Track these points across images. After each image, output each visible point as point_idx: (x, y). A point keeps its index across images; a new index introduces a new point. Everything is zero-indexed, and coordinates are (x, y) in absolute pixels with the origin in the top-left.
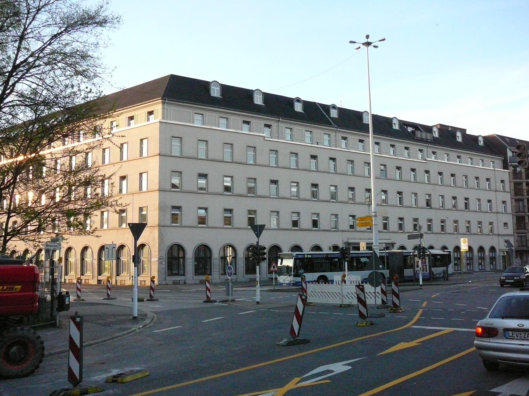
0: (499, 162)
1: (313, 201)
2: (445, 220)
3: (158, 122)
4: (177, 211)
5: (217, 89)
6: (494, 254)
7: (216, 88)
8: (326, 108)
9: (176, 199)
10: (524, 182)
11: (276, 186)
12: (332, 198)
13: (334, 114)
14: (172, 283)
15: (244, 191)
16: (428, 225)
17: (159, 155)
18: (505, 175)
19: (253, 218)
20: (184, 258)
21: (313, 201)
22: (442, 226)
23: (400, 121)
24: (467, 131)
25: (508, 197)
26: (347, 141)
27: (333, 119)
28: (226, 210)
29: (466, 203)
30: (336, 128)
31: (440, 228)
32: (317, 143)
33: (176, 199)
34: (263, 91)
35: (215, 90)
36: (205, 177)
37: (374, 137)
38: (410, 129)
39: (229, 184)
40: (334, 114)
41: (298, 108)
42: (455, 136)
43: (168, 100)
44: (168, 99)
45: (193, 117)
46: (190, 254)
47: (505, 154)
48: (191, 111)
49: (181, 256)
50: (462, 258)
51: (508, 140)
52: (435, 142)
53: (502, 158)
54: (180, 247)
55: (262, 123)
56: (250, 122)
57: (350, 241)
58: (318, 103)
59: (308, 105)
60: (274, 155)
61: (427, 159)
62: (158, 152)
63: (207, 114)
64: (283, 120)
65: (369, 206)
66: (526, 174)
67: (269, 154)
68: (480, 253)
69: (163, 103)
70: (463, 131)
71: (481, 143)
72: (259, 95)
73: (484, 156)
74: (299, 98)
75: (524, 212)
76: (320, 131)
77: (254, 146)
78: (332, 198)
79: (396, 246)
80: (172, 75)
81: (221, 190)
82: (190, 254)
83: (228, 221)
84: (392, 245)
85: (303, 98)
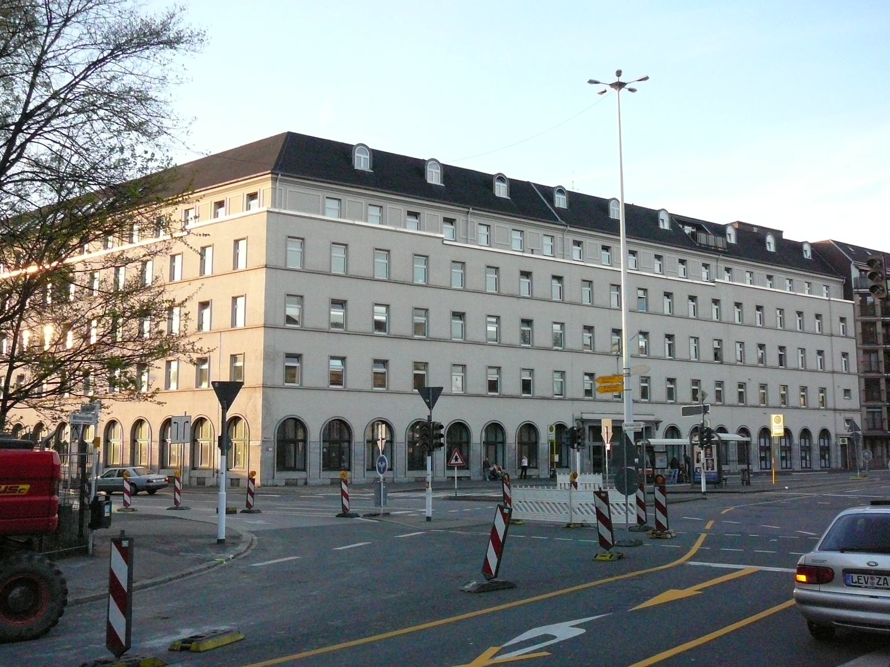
0: (836, 286)
1: (523, 348)
2: (745, 383)
3: (265, 212)
4: (293, 362)
5: (364, 158)
6: (767, 440)
7: (363, 156)
8: (548, 192)
9: (294, 342)
10: (878, 320)
11: (461, 322)
12: (555, 344)
13: (561, 202)
14: (284, 484)
15: (408, 331)
16: (717, 391)
17: (266, 266)
18: (848, 307)
19: (423, 375)
20: (305, 441)
21: (523, 348)
22: (741, 394)
23: (813, 245)
24: (783, 234)
25: (851, 346)
26: (582, 248)
27: (558, 210)
28: (376, 362)
29: (780, 356)
30: (563, 225)
31: (370, 378)
32: (532, 250)
33: (294, 342)
34: (441, 162)
35: (362, 159)
36: (342, 304)
37: (628, 242)
38: (688, 230)
39: (383, 318)
40: (561, 202)
41: (501, 191)
42: (763, 242)
43: (282, 175)
44: (282, 173)
45: (324, 205)
46: (315, 434)
47: (848, 274)
48: (321, 194)
49: (300, 438)
50: (773, 448)
51: (852, 250)
52: (730, 251)
53: (842, 280)
54: (298, 423)
55: (402, 209)
56: (419, 214)
57: (585, 417)
58: (534, 184)
59: (517, 187)
60: (383, 259)
61: (716, 280)
62: (263, 262)
63: (347, 199)
64: (283, 178)
65: (618, 359)
66: (882, 308)
67: (486, 273)
68: (822, 440)
69: (274, 180)
70: (777, 234)
71: (808, 255)
72: (436, 169)
73: (586, 234)
74: (500, 174)
75: (878, 372)
76: (315, 193)
77: (427, 255)
78: (555, 344)
79: (663, 428)
80: (289, 133)
81: (369, 327)
82: (315, 434)
83: (380, 380)
84: (655, 425)
85: (510, 175)
